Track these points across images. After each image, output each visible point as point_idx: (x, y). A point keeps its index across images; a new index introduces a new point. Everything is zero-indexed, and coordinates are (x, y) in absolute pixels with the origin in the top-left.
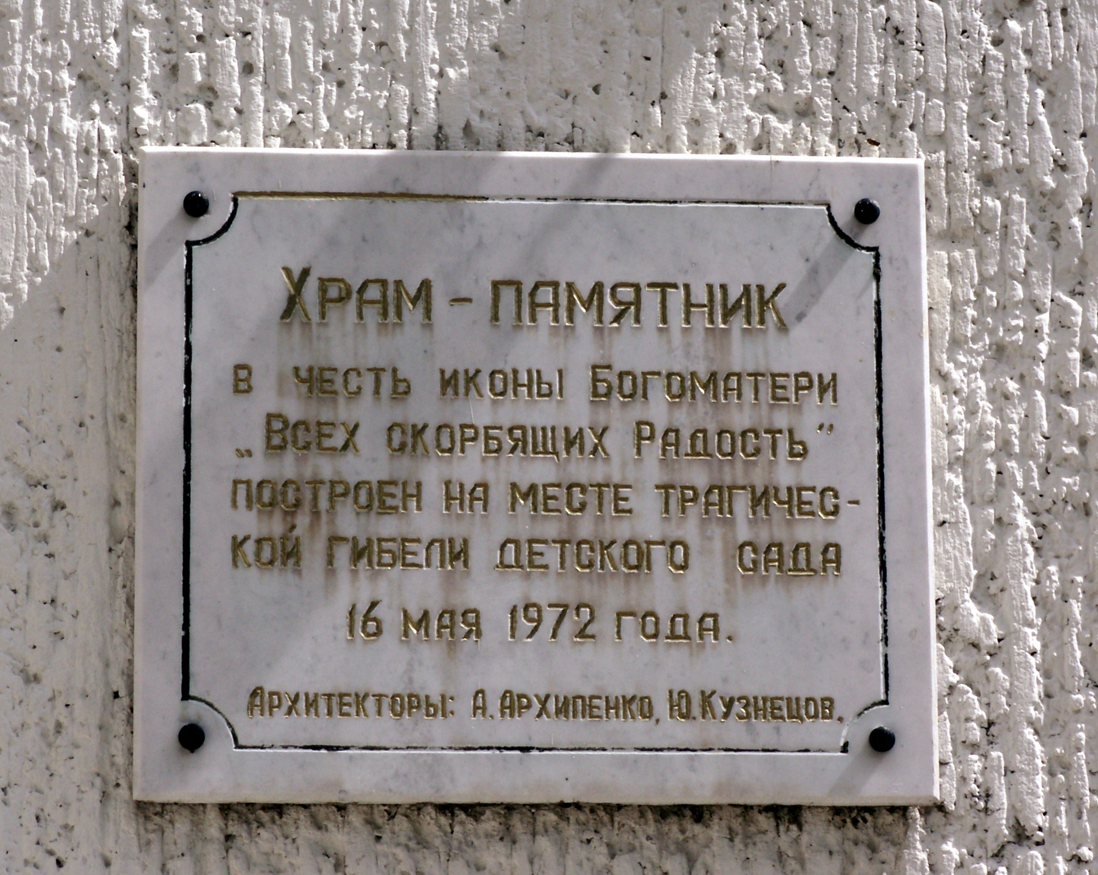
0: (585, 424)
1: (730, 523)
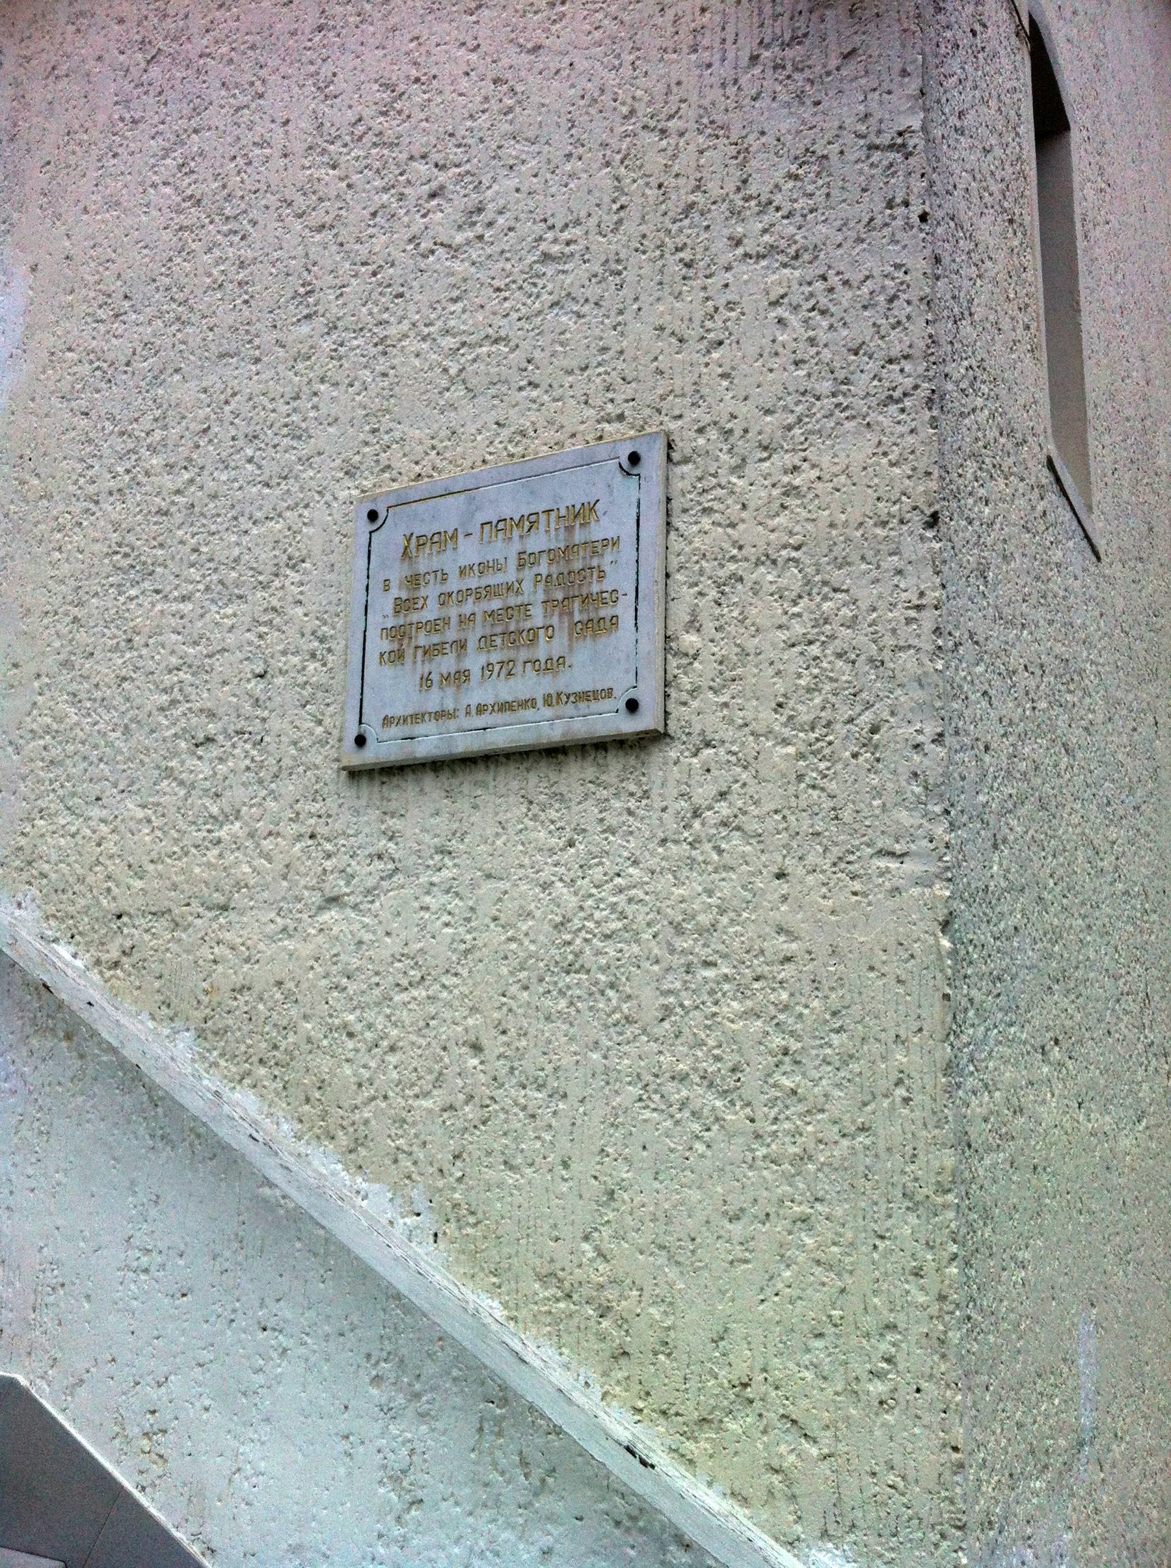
0: (8, 105)
1: (571, 614)
